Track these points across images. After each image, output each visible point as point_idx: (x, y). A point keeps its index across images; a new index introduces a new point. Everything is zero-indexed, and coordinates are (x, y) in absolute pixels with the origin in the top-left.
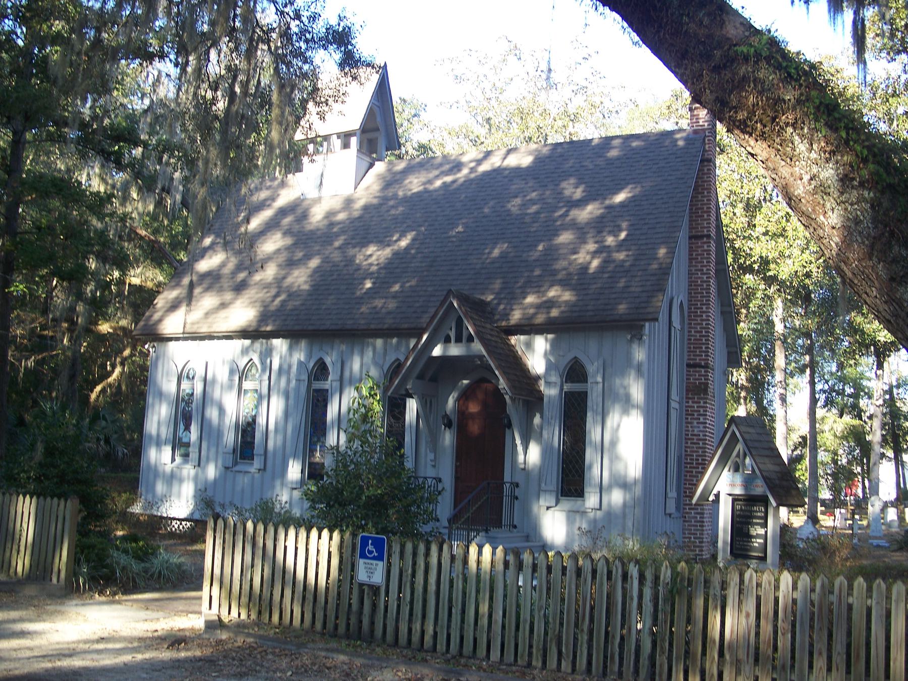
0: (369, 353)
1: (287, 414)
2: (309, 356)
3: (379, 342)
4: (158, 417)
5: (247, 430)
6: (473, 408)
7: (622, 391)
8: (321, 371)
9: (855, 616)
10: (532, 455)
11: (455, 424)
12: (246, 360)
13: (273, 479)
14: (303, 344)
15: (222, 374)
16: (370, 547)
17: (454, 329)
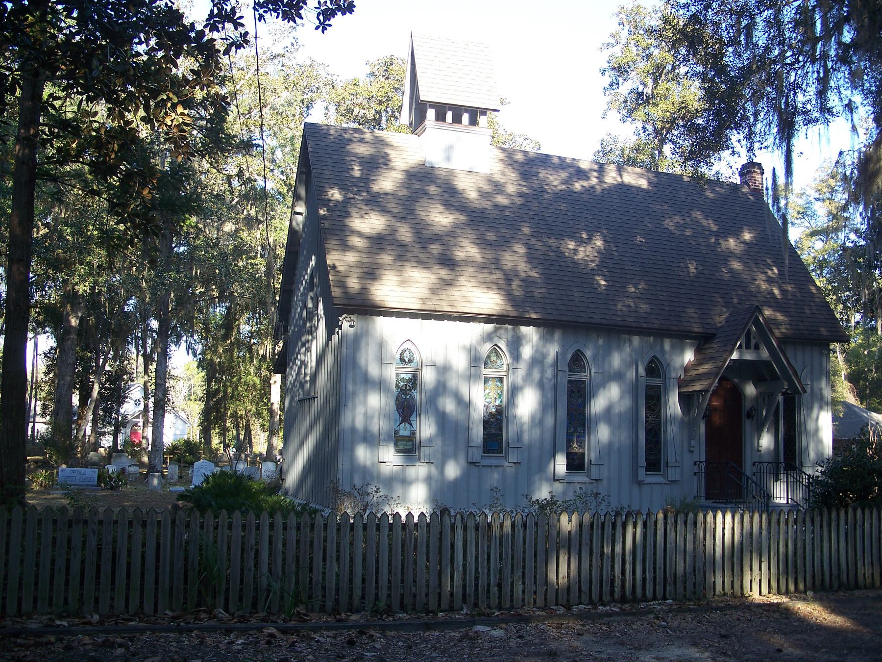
0: (628, 349)
1: (544, 407)
3: (636, 340)
4: (372, 407)
5: (496, 421)
8: (577, 361)
10: (766, 441)
11: (744, 414)
14: (557, 335)
15: (460, 362)
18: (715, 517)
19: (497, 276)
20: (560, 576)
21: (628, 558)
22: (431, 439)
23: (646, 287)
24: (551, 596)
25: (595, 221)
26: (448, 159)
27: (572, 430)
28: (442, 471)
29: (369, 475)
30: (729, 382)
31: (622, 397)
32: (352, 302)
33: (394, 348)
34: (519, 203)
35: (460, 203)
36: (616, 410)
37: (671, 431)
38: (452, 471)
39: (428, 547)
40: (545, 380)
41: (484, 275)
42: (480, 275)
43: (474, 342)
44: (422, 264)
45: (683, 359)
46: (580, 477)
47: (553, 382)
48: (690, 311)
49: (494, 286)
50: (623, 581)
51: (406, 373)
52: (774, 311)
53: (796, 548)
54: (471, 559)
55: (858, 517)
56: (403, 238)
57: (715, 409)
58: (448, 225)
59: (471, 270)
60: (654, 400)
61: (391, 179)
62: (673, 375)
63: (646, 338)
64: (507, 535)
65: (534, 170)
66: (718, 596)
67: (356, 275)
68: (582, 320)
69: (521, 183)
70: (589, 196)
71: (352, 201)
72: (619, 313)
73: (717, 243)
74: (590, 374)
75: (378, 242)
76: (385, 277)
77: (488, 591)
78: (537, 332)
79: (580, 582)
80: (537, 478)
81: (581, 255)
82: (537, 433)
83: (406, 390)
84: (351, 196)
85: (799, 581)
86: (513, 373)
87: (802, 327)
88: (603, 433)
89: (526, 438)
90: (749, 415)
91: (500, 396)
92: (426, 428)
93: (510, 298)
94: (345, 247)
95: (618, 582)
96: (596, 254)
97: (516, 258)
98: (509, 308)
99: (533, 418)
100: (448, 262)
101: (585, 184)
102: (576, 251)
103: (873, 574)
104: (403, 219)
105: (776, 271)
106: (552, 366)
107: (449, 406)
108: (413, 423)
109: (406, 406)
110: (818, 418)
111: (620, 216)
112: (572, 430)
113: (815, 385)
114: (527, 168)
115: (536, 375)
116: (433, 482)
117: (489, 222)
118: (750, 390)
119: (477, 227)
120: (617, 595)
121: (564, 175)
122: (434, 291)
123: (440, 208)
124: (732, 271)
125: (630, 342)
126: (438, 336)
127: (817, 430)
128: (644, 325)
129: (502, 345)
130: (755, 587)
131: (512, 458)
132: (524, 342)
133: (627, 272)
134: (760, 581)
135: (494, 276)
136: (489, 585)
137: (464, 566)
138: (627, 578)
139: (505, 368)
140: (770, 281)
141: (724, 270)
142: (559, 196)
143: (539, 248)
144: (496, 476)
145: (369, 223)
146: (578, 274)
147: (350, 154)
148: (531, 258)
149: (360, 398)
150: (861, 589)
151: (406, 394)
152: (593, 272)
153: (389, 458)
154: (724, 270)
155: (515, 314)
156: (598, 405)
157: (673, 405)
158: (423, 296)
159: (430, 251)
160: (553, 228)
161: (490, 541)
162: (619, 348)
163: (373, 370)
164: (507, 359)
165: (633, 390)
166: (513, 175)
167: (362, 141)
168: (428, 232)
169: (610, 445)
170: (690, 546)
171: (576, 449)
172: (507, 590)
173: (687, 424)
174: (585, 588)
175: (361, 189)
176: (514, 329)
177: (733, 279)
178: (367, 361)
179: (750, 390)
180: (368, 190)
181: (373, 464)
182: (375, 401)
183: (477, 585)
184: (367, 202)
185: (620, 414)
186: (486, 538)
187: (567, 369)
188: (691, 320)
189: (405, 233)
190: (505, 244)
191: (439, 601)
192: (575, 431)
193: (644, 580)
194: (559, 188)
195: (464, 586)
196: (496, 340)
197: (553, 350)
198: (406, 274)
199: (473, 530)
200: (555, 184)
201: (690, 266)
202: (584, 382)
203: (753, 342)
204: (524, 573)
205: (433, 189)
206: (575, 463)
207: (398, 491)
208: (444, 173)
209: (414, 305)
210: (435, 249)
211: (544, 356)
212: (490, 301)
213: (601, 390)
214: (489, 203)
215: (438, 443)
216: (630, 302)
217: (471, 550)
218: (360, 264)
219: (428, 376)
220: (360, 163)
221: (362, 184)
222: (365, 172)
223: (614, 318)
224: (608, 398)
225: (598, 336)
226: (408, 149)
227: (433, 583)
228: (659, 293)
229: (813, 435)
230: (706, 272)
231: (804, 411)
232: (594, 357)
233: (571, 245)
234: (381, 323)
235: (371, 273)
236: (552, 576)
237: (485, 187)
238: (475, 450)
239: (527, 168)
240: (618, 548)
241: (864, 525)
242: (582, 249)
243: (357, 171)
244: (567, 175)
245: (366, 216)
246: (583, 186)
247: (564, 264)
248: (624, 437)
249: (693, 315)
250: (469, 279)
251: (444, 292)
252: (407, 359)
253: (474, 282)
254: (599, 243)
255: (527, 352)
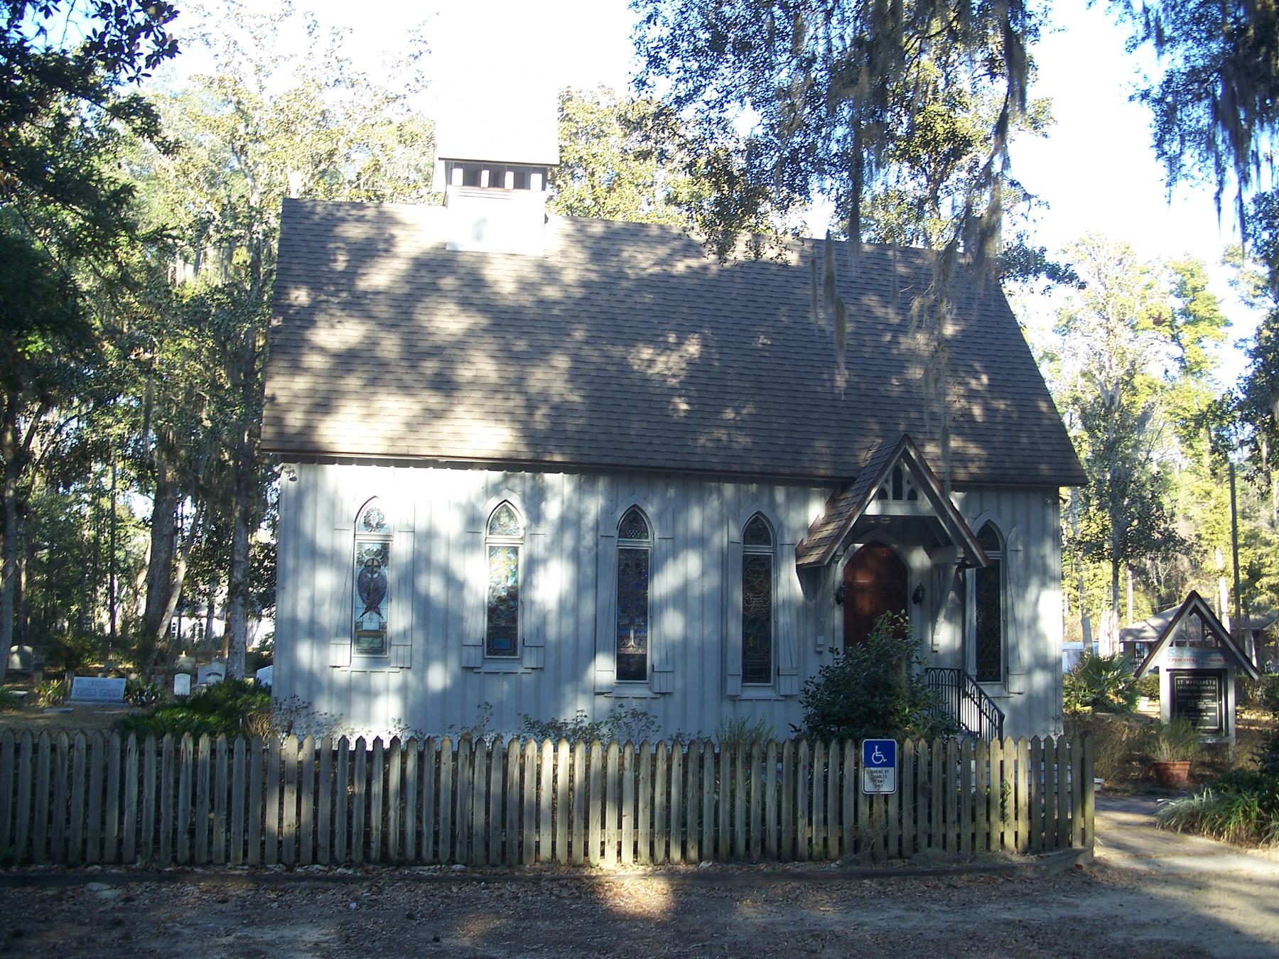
0: (715, 503)
1: (579, 588)
2: (612, 503)
3: (729, 489)
5: (505, 610)
6: (862, 580)
7: (1039, 562)
8: (634, 523)
9: (267, 849)
10: (945, 636)
12: (494, 502)
13: (558, 684)
14: (602, 484)
15: (451, 525)
16: (877, 753)
17: (891, 483)
18: (540, 749)
19: (517, 401)
20: (285, 823)
21: (393, 802)
22: (404, 634)
23: (754, 411)
24: (271, 849)
25: (696, 317)
26: (479, 237)
27: (627, 621)
28: (423, 677)
29: (315, 683)
30: (878, 547)
31: (704, 573)
32: (287, 446)
33: (350, 507)
34: (579, 296)
35: (484, 301)
36: (696, 591)
37: (783, 622)
38: (438, 678)
39: (87, 776)
40: (581, 549)
41: (497, 402)
42: (490, 404)
43: (473, 498)
44: (405, 389)
45: (806, 516)
46: (636, 691)
47: (594, 552)
48: (820, 445)
49: (506, 418)
50: (385, 835)
51: (371, 542)
52: (965, 441)
53: (684, 796)
54: (150, 793)
55: (801, 753)
56: (385, 354)
57: (862, 589)
58: (459, 333)
59: (477, 395)
60: (757, 574)
61: (389, 271)
62: (788, 540)
63: (743, 486)
64: (204, 763)
65: (616, 247)
66: (542, 863)
67: (303, 408)
68: (635, 463)
69: (591, 267)
70: (695, 281)
71: (324, 306)
72: (699, 450)
73: (895, 342)
74: (654, 539)
75: (346, 360)
76: (344, 411)
77: (175, 839)
78: (569, 480)
79: (315, 832)
80: (568, 689)
81: (659, 367)
82: (568, 625)
83: (373, 566)
84: (323, 297)
85: (689, 846)
86: (531, 540)
87: (1008, 465)
88: (672, 625)
89: (552, 632)
90: (917, 600)
91: (514, 574)
92: (397, 617)
93: (529, 434)
94: (296, 368)
95: (376, 835)
96: (684, 366)
97: (551, 376)
98: (522, 448)
99: (562, 604)
100: (445, 385)
101: (694, 263)
102: (651, 362)
103: (825, 839)
104: (392, 326)
105: (985, 379)
106: (592, 529)
107: (434, 586)
108: (383, 612)
109: (370, 586)
110: (1037, 600)
111: (739, 308)
112: (627, 621)
113: (1034, 551)
114: (604, 244)
115: (568, 540)
116: (410, 695)
117: (520, 327)
118: (919, 559)
119: (503, 334)
120: (375, 854)
121: (662, 251)
122: (412, 426)
123: (452, 307)
124: (907, 384)
125: (720, 492)
126: (418, 493)
127: (1035, 619)
128: (736, 468)
129: (515, 500)
130: (611, 851)
131: (530, 661)
132: (549, 496)
133: (729, 390)
134: (620, 844)
135: (511, 403)
136: (175, 831)
137: (140, 802)
138: (392, 830)
139: (522, 533)
140: (971, 395)
141: (895, 382)
142: (645, 283)
143: (594, 359)
144: (506, 686)
145: (341, 333)
146: (651, 396)
147: (337, 238)
148: (574, 376)
149: (305, 575)
150: (803, 860)
151: (373, 573)
152: (671, 392)
153: (344, 660)
154: (895, 382)
155: (529, 456)
156: (663, 584)
157: (789, 584)
158: (395, 434)
159: (421, 370)
160: (624, 330)
161: (177, 771)
162: (702, 502)
163: (323, 539)
164: (522, 519)
165: (723, 563)
166: (579, 256)
167: (360, 219)
168: (427, 344)
169: (685, 641)
170: (496, 789)
171: (632, 647)
172: (202, 837)
173: (811, 610)
174: (323, 841)
175: (341, 288)
176: (534, 478)
177: (906, 395)
178: (315, 526)
179: (919, 559)
180: (350, 288)
181: (323, 668)
182: (325, 581)
183: (157, 831)
184: (345, 306)
185: (702, 597)
186: (172, 766)
187: (615, 533)
188: (817, 458)
189: (390, 346)
190: (540, 356)
191: (102, 848)
192: (630, 624)
193: (419, 834)
194: (650, 271)
195: (139, 832)
196: (505, 494)
197: (594, 506)
198: (377, 405)
199: (153, 755)
200: (644, 265)
201: (838, 378)
202: (645, 552)
203: (906, 489)
204: (229, 816)
205: (448, 282)
206: (630, 670)
207: (359, 706)
208: (471, 259)
209: (378, 446)
210: (430, 366)
211: (580, 516)
212: (498, 438)
213: (670, 562)
214: (531, 298)
215: (419, 638)
216: (722, 434)
217: (151, 781)
218: (312, 392)
219: (402, 547)
220: (349, 251)
221: (343, 281)
222: (353, 263)
223: (690, 458)
224: (677, 575)
225: (667, 486)
226: (422, 227)
227: (94, 822)
228: (773, 419)
229: (1029, 627)
230: (863, 386)
231: (1012, 589)
232: (660, 516)
233: (647, 353)
234: (332, 473)
235: (324, 404)
236: (272, 822)
237: (531, 275)
238: (472, 650)
239: (604, 244)
240: (377, 788)
241: (811, 766)
242: (663, 358)
243: (341, 263)
244: (668, 251)
245: (339, 326)
246: (689, 267)
247: (627, 382)
248: (709, 631)
249: (824, 450)
250: (472, 408)
251: (428, 429)
252: (374, 524)
253: (477, 412)
254: (693, 348)
255: (553, 509)
